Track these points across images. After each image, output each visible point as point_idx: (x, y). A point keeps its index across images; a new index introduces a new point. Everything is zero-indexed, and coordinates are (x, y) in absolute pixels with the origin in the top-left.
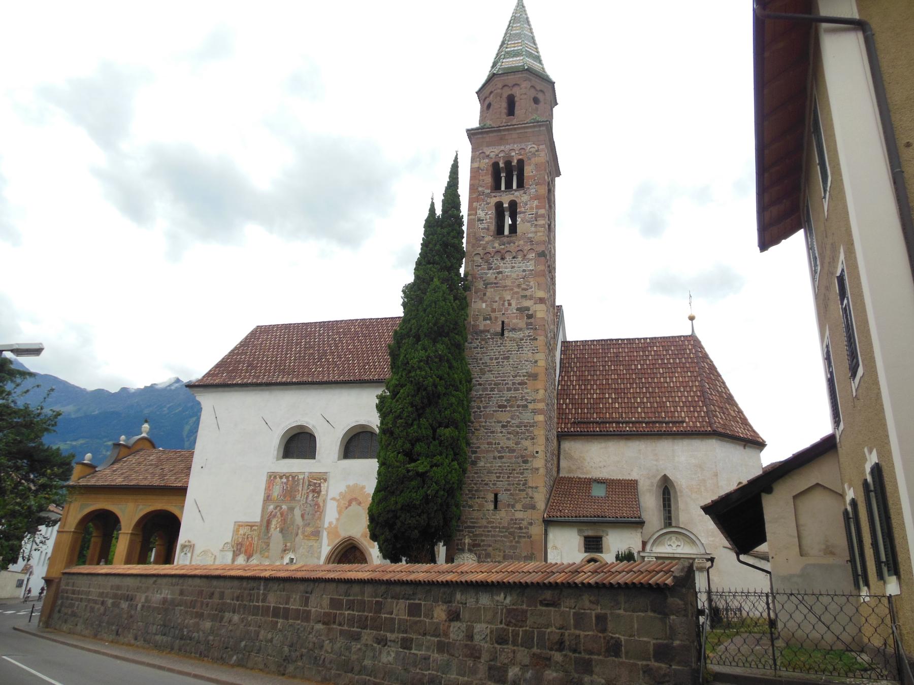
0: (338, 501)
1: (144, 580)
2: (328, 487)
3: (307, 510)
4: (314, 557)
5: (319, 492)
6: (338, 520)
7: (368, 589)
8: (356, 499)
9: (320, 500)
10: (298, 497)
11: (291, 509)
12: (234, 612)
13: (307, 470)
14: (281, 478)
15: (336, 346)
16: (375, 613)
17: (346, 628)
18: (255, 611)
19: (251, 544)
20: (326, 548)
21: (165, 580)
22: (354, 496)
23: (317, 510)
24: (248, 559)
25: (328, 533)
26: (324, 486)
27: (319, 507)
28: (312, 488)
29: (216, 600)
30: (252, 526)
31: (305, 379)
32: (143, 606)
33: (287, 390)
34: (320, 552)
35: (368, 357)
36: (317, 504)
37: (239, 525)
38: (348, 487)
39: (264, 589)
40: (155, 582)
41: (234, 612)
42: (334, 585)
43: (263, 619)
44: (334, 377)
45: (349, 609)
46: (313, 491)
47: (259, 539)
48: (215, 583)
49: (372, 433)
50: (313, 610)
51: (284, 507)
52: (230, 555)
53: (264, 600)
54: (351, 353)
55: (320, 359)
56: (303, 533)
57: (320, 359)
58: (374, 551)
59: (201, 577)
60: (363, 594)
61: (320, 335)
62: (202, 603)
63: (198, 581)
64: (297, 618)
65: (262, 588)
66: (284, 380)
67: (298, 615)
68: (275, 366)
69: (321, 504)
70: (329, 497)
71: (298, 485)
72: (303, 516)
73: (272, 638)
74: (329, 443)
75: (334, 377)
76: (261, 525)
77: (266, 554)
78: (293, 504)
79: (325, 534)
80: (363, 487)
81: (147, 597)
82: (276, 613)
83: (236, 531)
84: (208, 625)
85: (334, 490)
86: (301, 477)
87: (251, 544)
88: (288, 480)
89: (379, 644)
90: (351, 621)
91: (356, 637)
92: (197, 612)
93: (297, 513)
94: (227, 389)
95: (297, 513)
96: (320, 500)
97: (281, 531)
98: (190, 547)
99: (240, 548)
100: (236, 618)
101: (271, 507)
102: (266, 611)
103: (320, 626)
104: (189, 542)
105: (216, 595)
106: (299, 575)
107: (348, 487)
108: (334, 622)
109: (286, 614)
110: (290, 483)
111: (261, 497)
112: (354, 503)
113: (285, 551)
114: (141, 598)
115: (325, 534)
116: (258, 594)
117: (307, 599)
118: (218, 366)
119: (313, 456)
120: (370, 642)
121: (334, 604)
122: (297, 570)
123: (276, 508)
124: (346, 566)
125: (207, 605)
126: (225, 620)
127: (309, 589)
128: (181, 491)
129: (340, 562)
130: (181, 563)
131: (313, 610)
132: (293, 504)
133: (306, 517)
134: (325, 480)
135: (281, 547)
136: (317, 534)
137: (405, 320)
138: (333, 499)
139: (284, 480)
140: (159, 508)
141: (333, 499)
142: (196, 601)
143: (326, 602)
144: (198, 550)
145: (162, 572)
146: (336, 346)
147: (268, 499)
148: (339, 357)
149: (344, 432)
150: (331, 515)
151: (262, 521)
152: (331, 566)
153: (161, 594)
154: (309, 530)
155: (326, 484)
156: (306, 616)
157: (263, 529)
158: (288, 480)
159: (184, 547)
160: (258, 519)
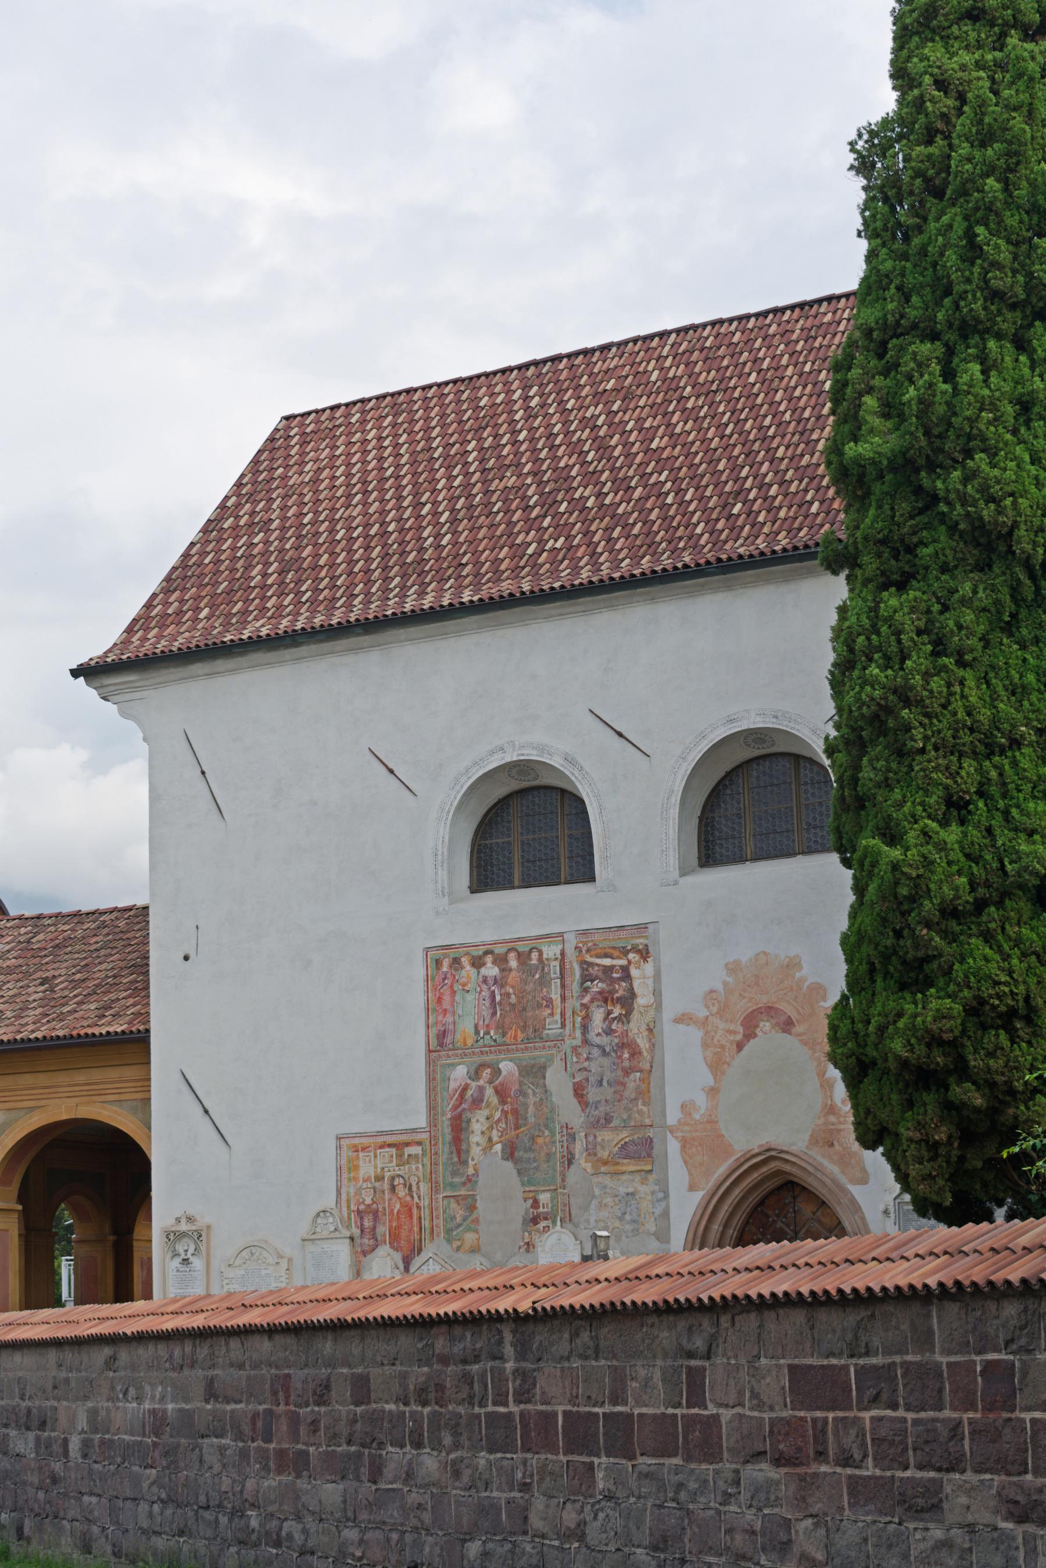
0: (704, 1023)
1: (68, 1356)
2: (657, 976)
3: (594, 1067)
4: (645, 1235)
5: (628, 1001)
6: (713, 1092)
7: (940, 1321)
8: (770, 1011)
9: (636, 1028)
10: (552, 1027)
11: (535, 1072)
12: (418, 1445)
13: (569, 926)
14: (477, 963)
15: (603, 448)
16: (990, 1407)
17: (870, 1470)
18: (499, 1435)
19: (408, 1209)
20: (685, 1205)
21: (145, 1353)
22: (763, 1000)
23: (632, 1062)
24: (407, 1262)
25: (685, 1144)
26: (642, 975)
27: (636, 1053)
28: (597, 986)
29: (342, 1407)
30: (399, 1146)
31: (507, 586)
32: (86, 1444)
33: (444, 635)
34: (666, 1214)
35: (735, 468)
36: (627, 1045)
37: (353, 1148)
38: (733, 968)
39: (521, 1356)
40: (110, 1363)
41: (418, 1445)
42: (799, 1317)
43: (534, 1460)
44: (616, 564)
45: (875, 1400)
46: (605, 998)
47: (434, 1189)
48: (327, 1346)
49: (799, 759)
50: (726, 1415)
51: (507, 1067)
52: (342, 1252)
53: (523, 1396)
54: (662, 464)
55: (549, 504)
56: (591, 1152)
57: (549, 504)
58: (873, 1187)
59: (272, 1331)
60: (925, 1341)
61: (529, 417)
62: (294, 1420)
63: (265, 1346)
64: (666, 1451)
65: (508, 1350)
66: (427, 602)
67: (665, 1438)
68: (385, 556)
69: (643, 1043)
70: (670, 1009)
71: (544, 982)
72: (579, 1091)
73: (582, 1524)
74: (638, 816)
75: (616, 564)
76: (433, 1140)
77: (470, 1238)
78: (538, 1054)
79: (673, 1147)
80: (793, 964)
81: (93, 1413)
82: (581, 1435)
83: (347, 1170)
84: (331, 1492)
85: (680, 986)
86: (551, 951)
87: (408, 1209)
88: (505, 970)
89: (1021, 1520)
90: (890, 1447)
91: (926, 1504)
92: (281, 1453)
93: (558, 1081)
94: (221, 664)
95: (558, 1081)
96: (636, 1028)
97: (510, 1152)
98: (192, 1236)
99: (374, 1224)
100: (430, 1463)
101: (460, 1073)
102: (539, 1432)
103: (764, 1471)
104: (190, 1219)
105: (341, 1391)
106: (646, 1294)
107: (733, 968)
108: (821, 1455)
109: (622, 1436)
110: (513, 977)
111: (415, 1042)
112: (765, 1025)
113: (535, 1220)
114: (74, 1418)
115: (673, 1147)
116: (499, 1377)
117: (696, 1378)
118: (171, 583)
119: (582, 869)
120: (983, 1517)
121: (806, 1385)
122: (632, 1278)
123: (476, 1075)
124: (761, 1252)
125: (315, 1423)
126: (388, 1472)
127: (699, 1343)
128: (135, 1045)
129: (742, 1241)
130: (172, 1292)
131: (726, 1415)
132: (538, 1054)
133: (593, 1094)
134: (644, 954)
135: (520, 1208)
136: (641, 1150)
137: (874, 284)
138: (682, 1019)
139: (491, 970)
140: (64, 1117)
141: (682, 1019)
142: (269, 1412)
143: (774, 1381)
144: (224, 1245)
145: (130, 1328)
146: (603, 448)
147: (441, 1043)
148: (622, 485)
149: (687, 768)
150: (683, 1075)
151: (433, 1122)
152: (710, 1257)
153: (139, 1399)
154: (610, 1139)
155: (649, 968)
156: (705, 1441)
157: (444, 1150)
158: (505, 970)
159: (173, 1237)
160: (421, 1121)
